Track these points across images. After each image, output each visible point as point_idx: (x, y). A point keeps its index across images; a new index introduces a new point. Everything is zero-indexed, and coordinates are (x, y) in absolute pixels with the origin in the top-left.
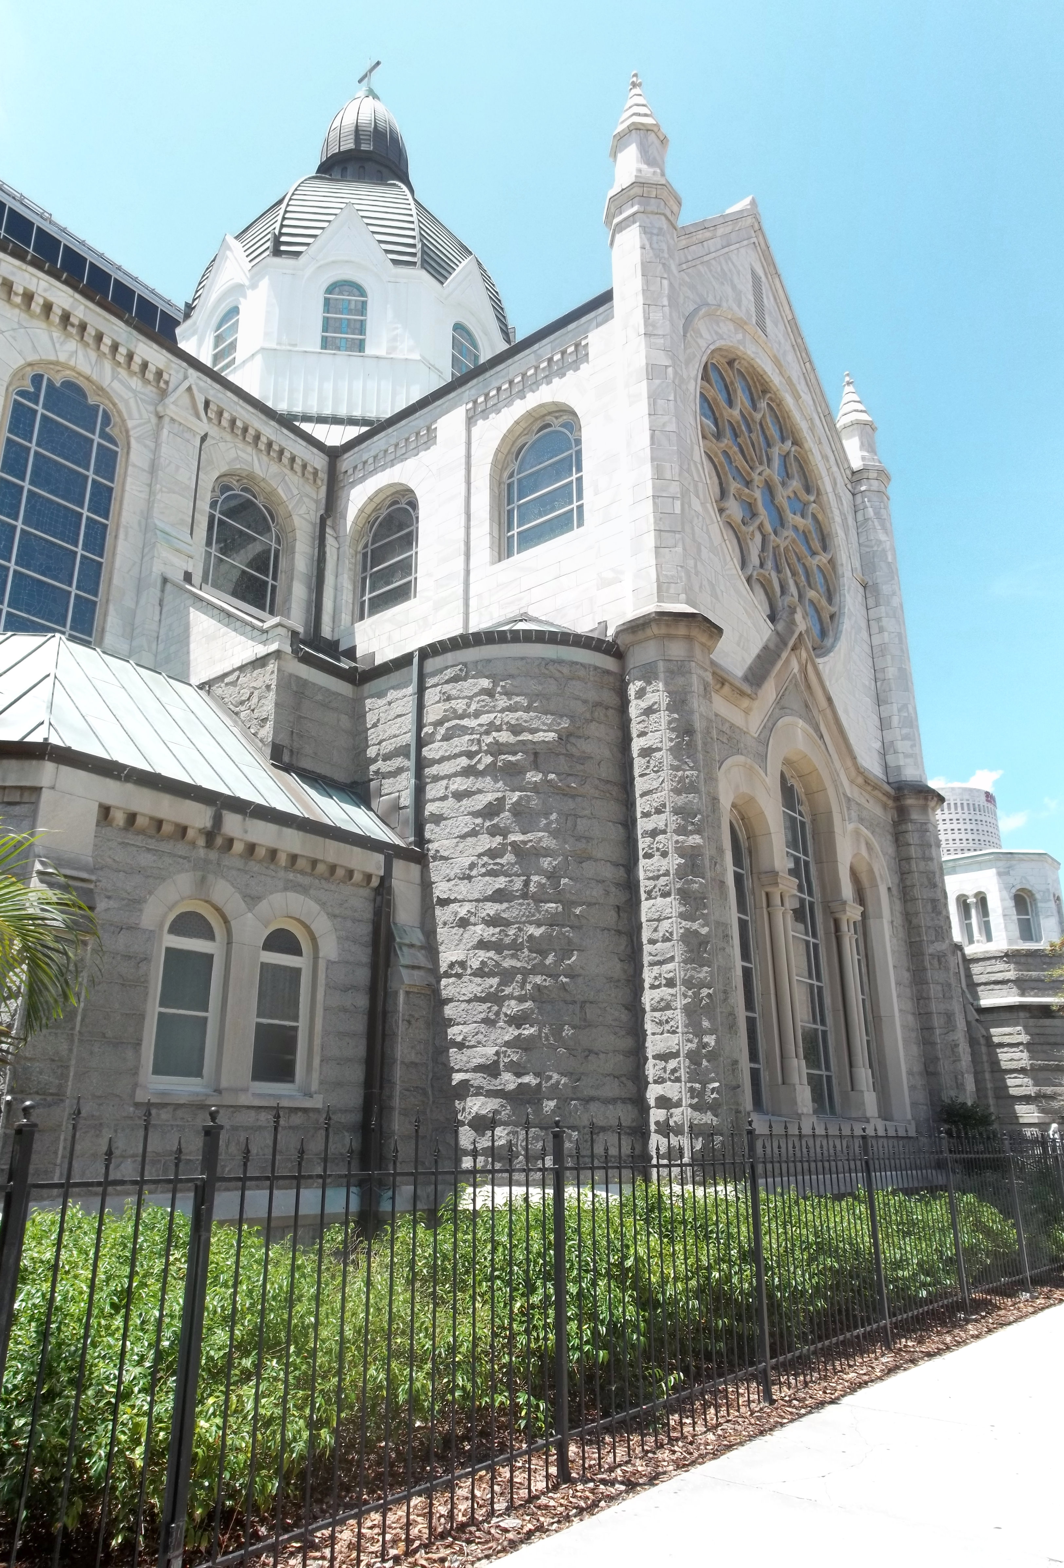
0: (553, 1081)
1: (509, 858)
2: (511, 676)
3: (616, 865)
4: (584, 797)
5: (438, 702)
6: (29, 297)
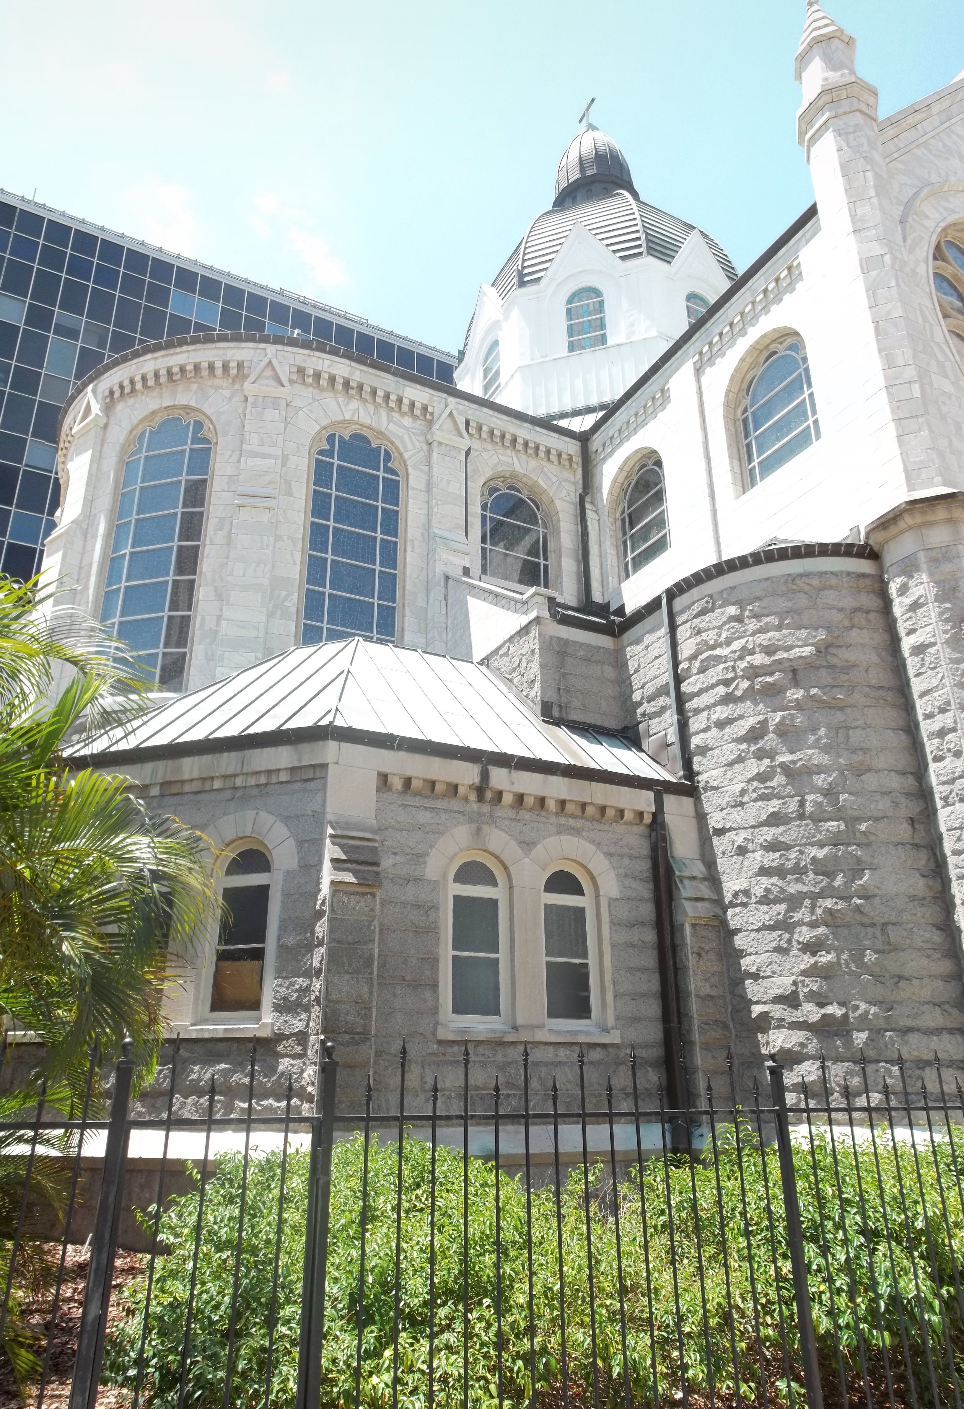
0: (861, 1011)
1: (779, 780)
2: (758, 599)
3: (903, 773)
4: (854, 707)
5: (690, 637)
6: (317, 375)
